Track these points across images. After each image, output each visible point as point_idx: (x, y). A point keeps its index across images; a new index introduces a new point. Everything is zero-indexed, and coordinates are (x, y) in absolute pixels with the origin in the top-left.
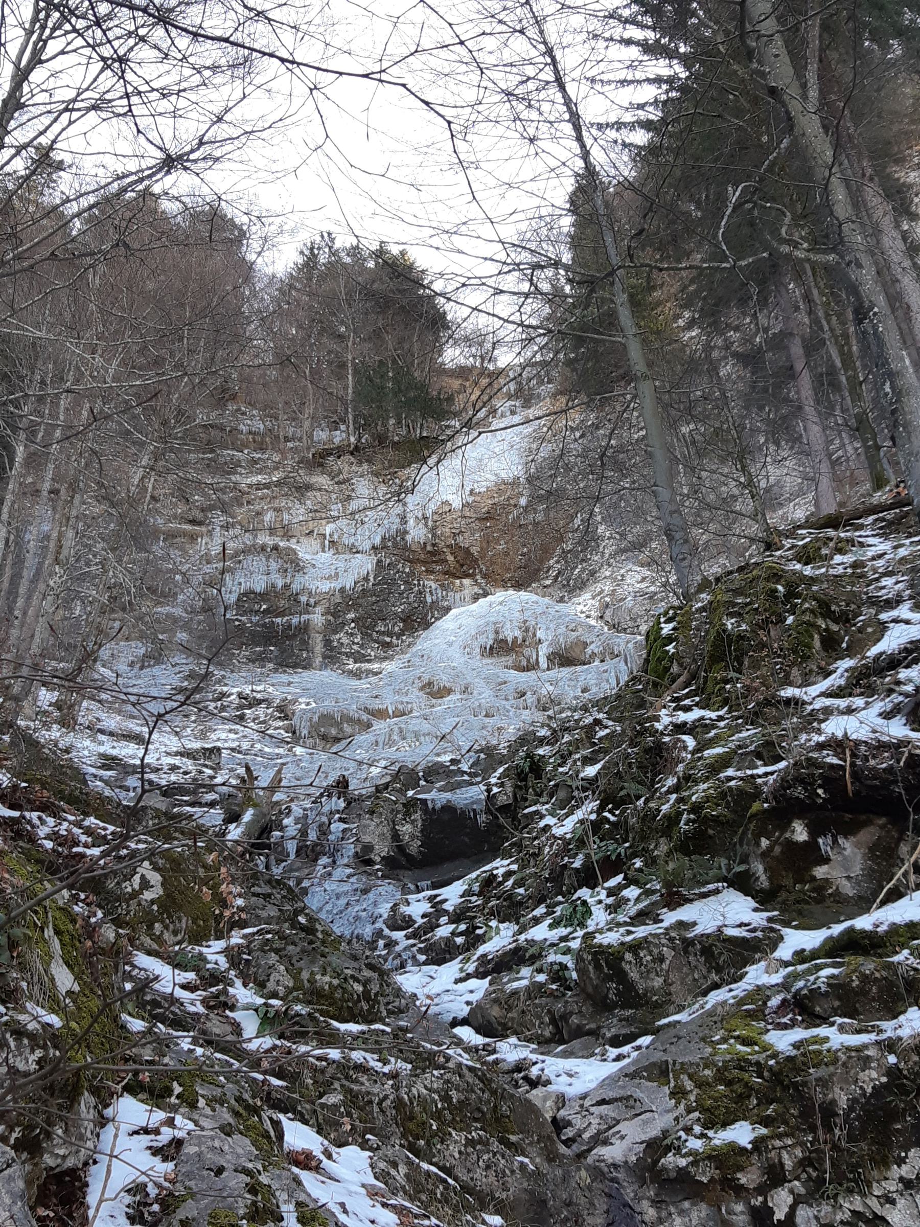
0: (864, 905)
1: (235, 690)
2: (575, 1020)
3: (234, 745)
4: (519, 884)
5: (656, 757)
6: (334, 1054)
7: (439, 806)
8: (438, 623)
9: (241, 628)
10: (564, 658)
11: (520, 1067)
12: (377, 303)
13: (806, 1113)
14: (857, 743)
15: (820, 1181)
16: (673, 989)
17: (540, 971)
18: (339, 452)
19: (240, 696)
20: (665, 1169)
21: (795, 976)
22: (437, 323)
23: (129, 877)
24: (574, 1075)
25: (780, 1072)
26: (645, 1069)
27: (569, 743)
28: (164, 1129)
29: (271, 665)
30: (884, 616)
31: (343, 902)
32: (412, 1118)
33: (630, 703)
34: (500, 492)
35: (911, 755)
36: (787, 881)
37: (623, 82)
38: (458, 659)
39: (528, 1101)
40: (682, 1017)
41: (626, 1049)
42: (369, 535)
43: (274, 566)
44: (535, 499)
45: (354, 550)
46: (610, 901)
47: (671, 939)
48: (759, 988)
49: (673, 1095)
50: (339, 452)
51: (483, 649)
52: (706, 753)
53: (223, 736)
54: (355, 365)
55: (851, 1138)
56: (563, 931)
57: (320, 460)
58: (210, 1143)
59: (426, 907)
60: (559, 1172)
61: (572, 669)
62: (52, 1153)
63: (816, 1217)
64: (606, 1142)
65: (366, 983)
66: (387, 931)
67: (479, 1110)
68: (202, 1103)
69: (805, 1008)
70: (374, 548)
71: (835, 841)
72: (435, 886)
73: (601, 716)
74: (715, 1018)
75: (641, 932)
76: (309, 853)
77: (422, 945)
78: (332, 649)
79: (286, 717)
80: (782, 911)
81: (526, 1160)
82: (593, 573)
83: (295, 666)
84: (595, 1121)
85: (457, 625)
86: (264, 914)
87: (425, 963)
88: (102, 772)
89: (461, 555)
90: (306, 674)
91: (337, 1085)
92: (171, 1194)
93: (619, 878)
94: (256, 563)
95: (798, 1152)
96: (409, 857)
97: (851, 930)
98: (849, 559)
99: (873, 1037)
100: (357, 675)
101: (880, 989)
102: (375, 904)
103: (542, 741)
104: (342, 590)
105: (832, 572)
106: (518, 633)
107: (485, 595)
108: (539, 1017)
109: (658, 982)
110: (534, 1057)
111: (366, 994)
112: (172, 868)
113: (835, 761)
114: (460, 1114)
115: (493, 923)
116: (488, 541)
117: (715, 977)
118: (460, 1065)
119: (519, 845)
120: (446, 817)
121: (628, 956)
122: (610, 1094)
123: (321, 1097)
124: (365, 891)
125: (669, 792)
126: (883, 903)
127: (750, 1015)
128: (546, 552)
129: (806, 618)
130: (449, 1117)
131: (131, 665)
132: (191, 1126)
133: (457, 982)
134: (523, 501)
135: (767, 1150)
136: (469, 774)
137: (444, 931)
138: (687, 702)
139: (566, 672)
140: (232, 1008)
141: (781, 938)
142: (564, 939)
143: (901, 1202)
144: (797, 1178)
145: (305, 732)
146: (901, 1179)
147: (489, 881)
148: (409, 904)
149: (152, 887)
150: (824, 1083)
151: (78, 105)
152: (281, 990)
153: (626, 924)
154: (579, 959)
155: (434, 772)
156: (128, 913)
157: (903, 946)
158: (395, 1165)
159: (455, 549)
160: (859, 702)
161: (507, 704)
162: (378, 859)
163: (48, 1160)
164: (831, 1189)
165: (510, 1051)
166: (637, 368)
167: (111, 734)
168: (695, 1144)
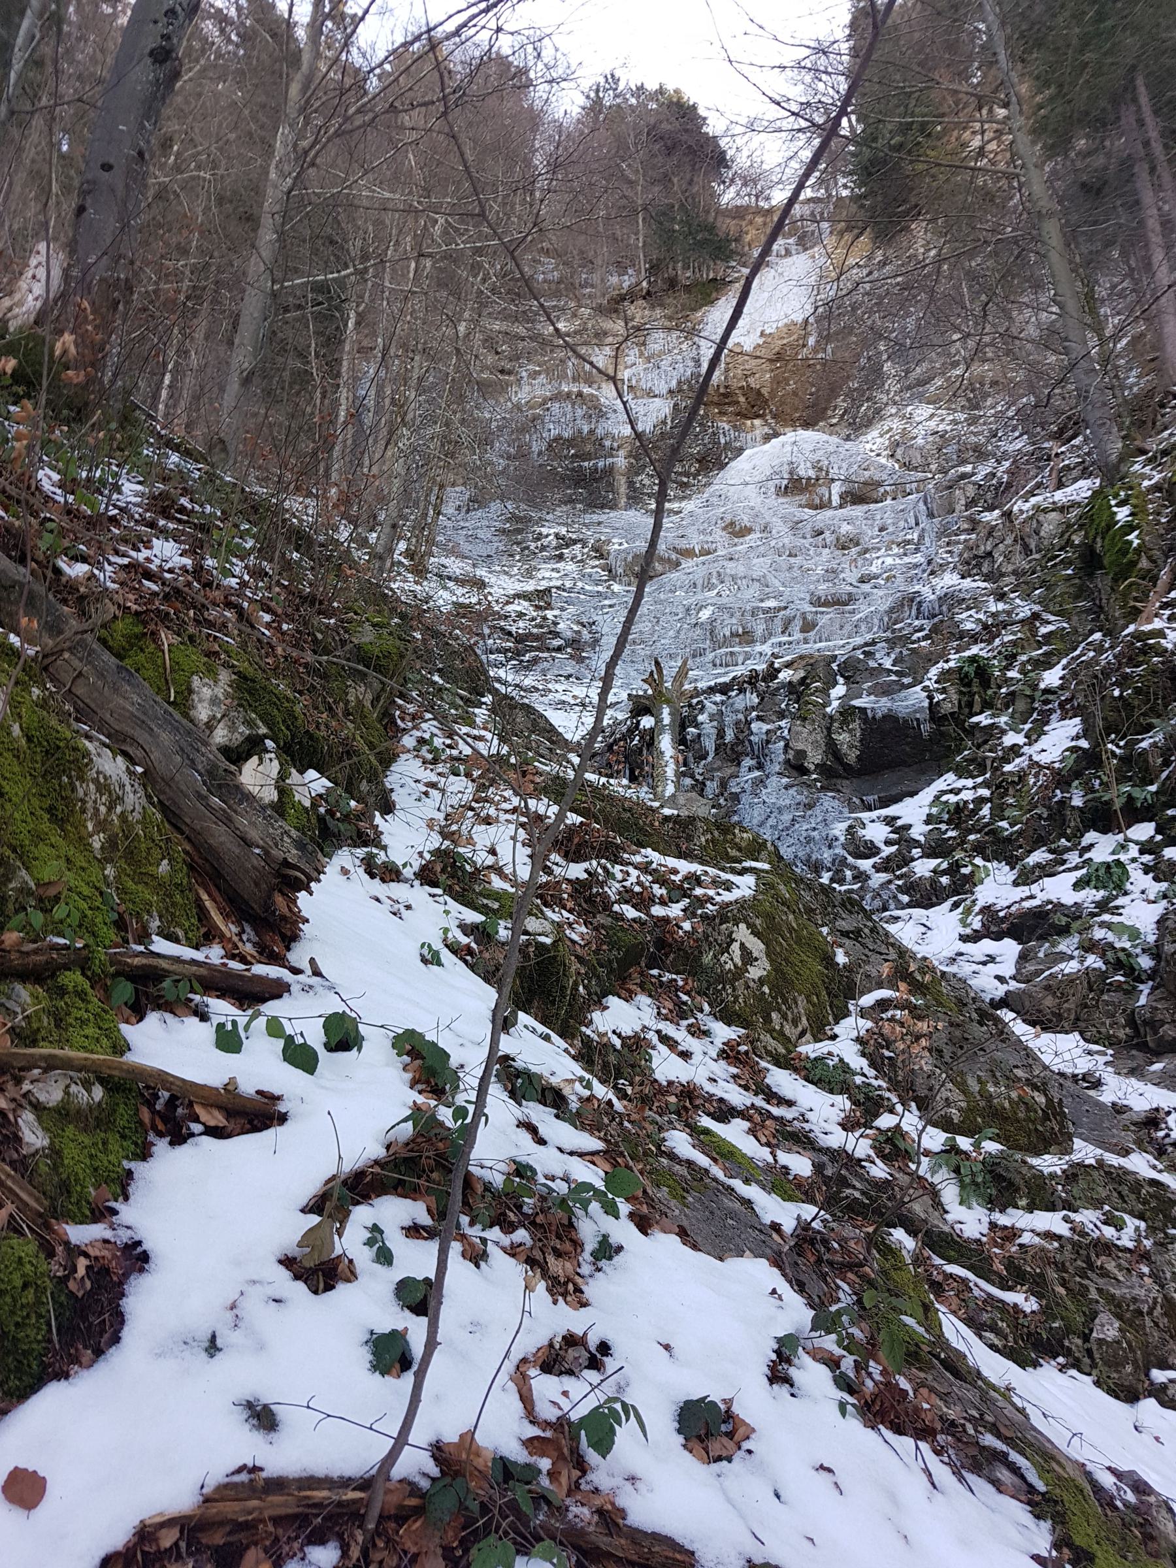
1: (552, 531)
3: (559, 583)
7: (879, 715)
8: (733, 464)
18: (631, 296)
19: (557, 536)
22: (720, 160)
31: (787, 817)
34: (790, 333)
44: (825, 338)
45: (651, 394)
57: (616, 305)
61: (865, 507)
66: (850, 859)
70: (670, 392)
72: (885, 803)
77: (900, 883)
79: (601, 557)
82: (878, 411)
85: (751, 465)
87: (910, 905)
89: (752, 396)
96: (847, 767)
106: (812, 473)
107: (776, 435)
116: (778, 382)
120: (887, 726)
124: (809, 806)
128: (833, 392)
131: (459, 508)
134: (811, 341)
136: (896, 673)
139: (858, 511)
145: (620, 571)
148: (864, 826)
149: (756, 959)
156: (736, 998)
159: (747, 390)
161: (806, 542)
162: (812, 767)
166: (1041, 203)
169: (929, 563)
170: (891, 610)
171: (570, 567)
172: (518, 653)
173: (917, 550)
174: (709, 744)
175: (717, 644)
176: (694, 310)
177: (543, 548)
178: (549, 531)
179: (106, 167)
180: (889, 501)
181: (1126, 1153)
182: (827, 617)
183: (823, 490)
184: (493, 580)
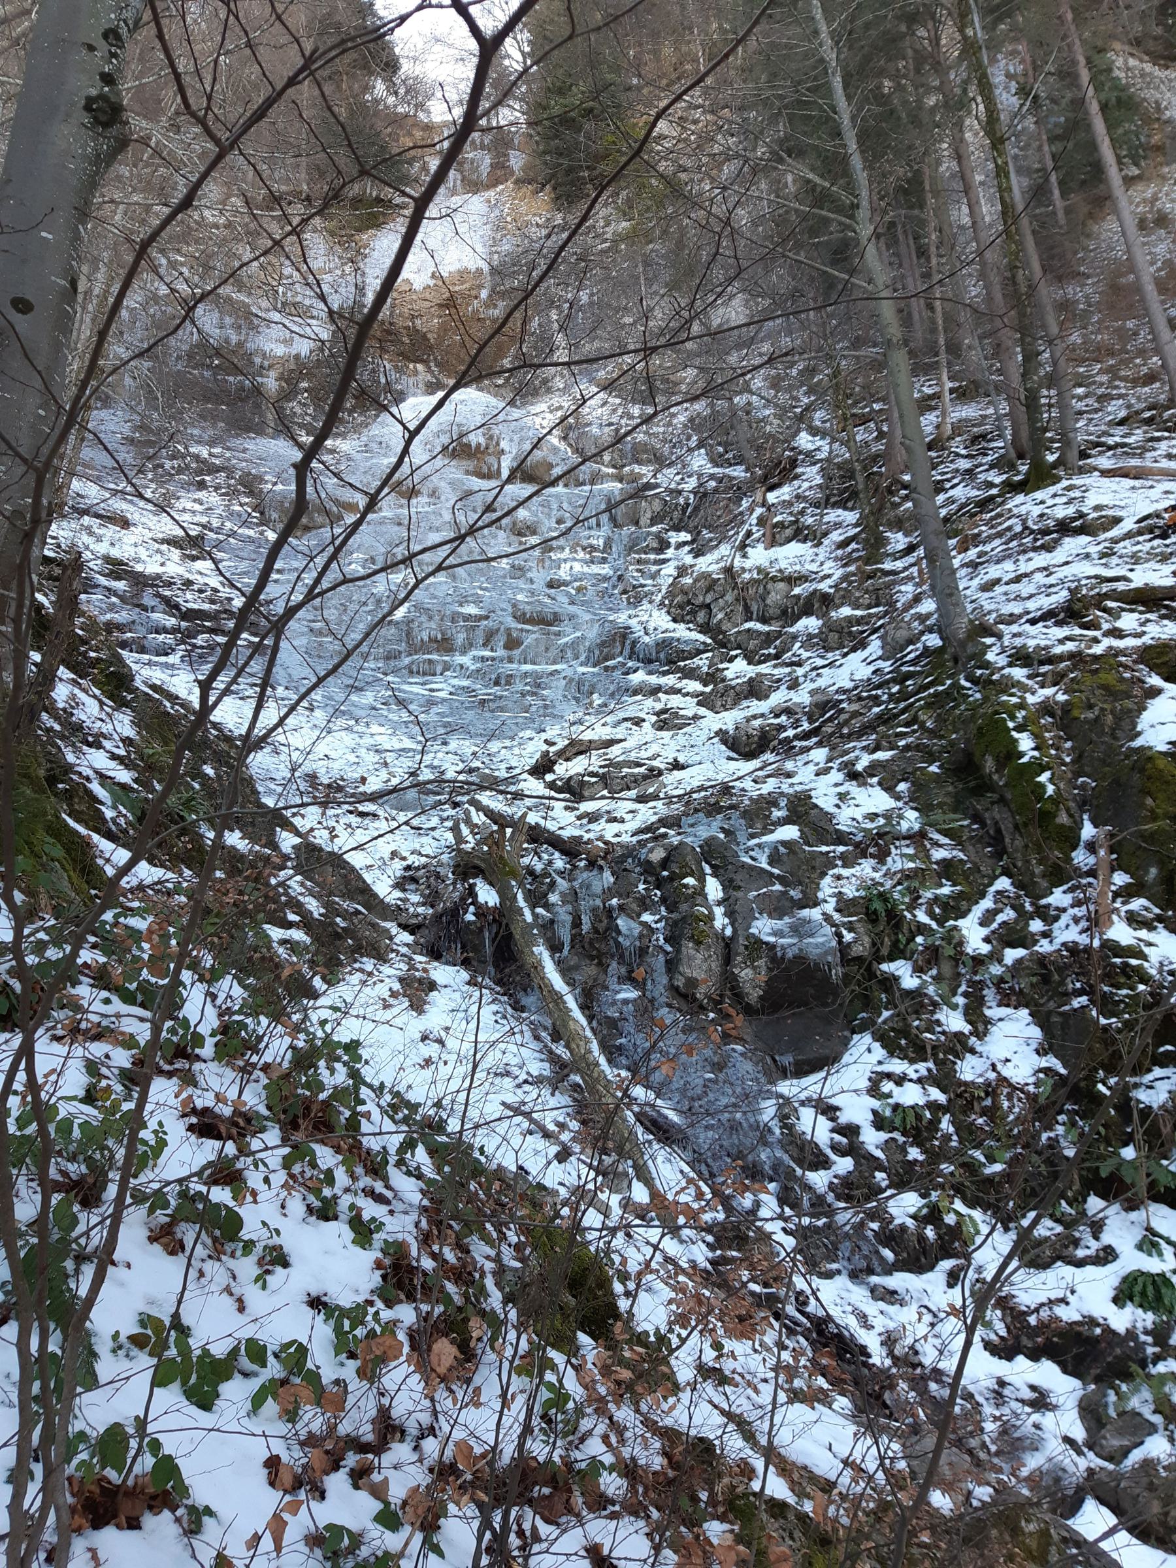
3: (204, 520)
43: (228, 320)
83: (249, 430)
116: (444, 329)
134: (484, 294)
159: (414, 332)
169: (620, 578)
170: (603, 645)
171: (213, 499)
173: (604, 561)
175: (414, 649)
176: (360, 230)
177: (180, 471)
179: (23, 306)
182: (532, 636)
183: (492, 460)
184: (136, 516)
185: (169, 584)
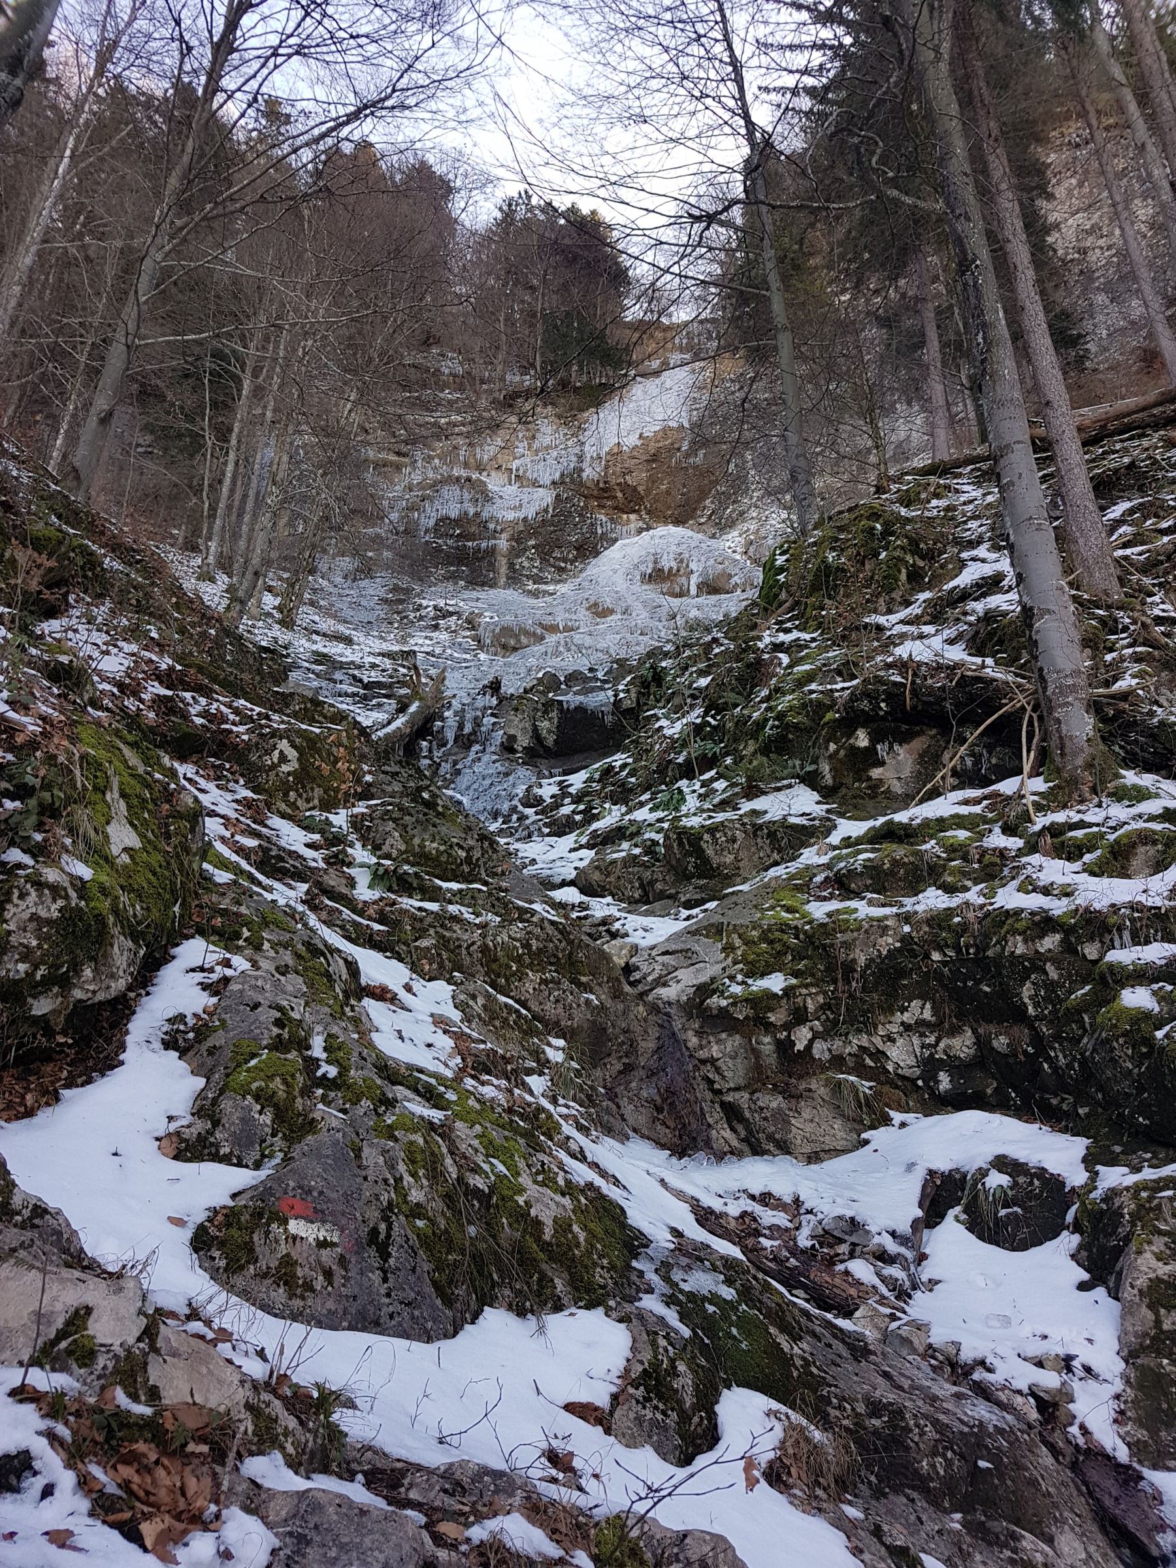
0: (906, 801)
2: (659, 886)
3: (429, 649)
4: (632, 774)
5: (754, 672)
6: (433, 907)
9: (438, 550)
10: (711, 587)
11: (605, 922)
12: (566, 258)
13: (830, 969)
14: (920, 664)
15: (835, 1023)
16: (741, 864)
17: (636, 846)
18: (528, 394)
19: (435, 608)
20: (709, 1008)
21: (839, 858)
22: (619, 277)
23: (269, 752)
24: (651, 931)
25: (813, 936)
26: (705, 928)
27: (689, 657)
28: (218, 968)
29: (462, 583)
30: (964, 555)
31: (488, 782)
32: (496, 960)
33: (742, 627)
35: (963, 676)
36: (848, 780)
37: (792, 47)
38: (621, 585)
39: (603, 951)
40: (745, 887)
41: (694, 912)
42: (549, 472)
43: (466, 496)
45: (535, 484)
46: (702, 791)
47: (743, 824)
48: (808, 867)
49: (724, 949)
50: (528, 394)
51: (643, 575)
52: (795, 669)
53: (419, 642)
54: (544, 316)
55: (864, 989)
56: (660, 814)
57: (509, 401)
58: (253, 982)
59: (555, 790)
60: (621, 1007)
61: (718, 597)
62: (82, 988)
63: (829, 1050)
64: (665, 985)
65: (469, 850)
66: (520, 808)
67: (555, 956)
68: (266, 946)
69: (843, 884)
70: (554, 483)
71: (891, 748)
72: (565, 773)
73: (720, 635)
74: (768, 890)
75: (720, 817)
76: (465, 742)
78: (515, 571)
79: (473, 628)
80: (840, 805)
81: (593, 997)
82: (742, 514)
83: (483, 584)
84: (658, 968)
86: (389, 789)
87: (548, 835)
88: (314, 667)
89: (629, 491)
90: (492, 592)
91: (432, 931)
92: (206, 1025)
93: (713, 773)
94: (451, 493)
95: (821, 999)
96: (547, 749)
97: (891, 822)
98: (943, 503)
99: (895, 910)
100: (535, 594)
101: (907, 873)
102: (514, 785)
103: (666, 655)
104: (525, 519)
105: (927, 514)
106: (674, 564)
107: (648, 529)
108: (631, 882)
109: (729, 859)
110: (618, 915)
111: (468, 860)
112: (309, 747)
113: (899, 679)
114: (539, 958)
115: (607, 805)
116: (653, 480)
117: (776, 856)
118: (543, 919)
119: (636, 742)
121: (706, 837)
122: (674, 947)
123: (416, 940)
124: (507, 775)
125: (761, 702)
126: (921, 802)
127: (798, 888)
128: (703, 495)
129: (897, 553)
130: (528, 961)
132: (247, 965)
133: (572, 850)
135: (795, 996)
137: (566, 810)
138: (789, 625)
140: (349, 865)
141: (835, 827)
142: (660, 820)
143: (900, 1042)
144: (818, 1019)
145: (488, 641)
146: (903, 1023)
147: (608, 771)
150: (847, 945)
151: (281, 51)
152: (395, 853)
153: (709, 810)
154: (666, 837)
155: (573, 678)
157: (931, 837)
158: (474, 997)
159: (624, 487)
160: (928, 629)
163: (78, 994)
164: (843, 1029)
165: (601, 908)
167: (324, 635)
168: (736, 989)
172: (365, 698)
174: (450, 735)
177: (421, 618)
178: (429, 603)
180: (739, 592)
181: (532, 902)
185: (359, 667)
